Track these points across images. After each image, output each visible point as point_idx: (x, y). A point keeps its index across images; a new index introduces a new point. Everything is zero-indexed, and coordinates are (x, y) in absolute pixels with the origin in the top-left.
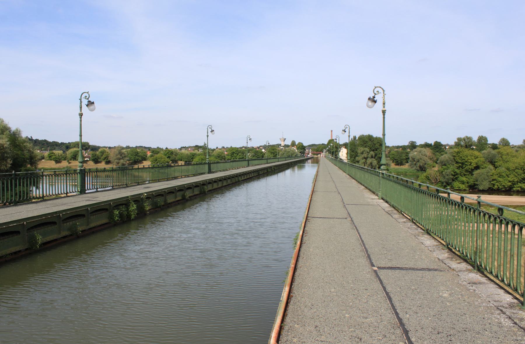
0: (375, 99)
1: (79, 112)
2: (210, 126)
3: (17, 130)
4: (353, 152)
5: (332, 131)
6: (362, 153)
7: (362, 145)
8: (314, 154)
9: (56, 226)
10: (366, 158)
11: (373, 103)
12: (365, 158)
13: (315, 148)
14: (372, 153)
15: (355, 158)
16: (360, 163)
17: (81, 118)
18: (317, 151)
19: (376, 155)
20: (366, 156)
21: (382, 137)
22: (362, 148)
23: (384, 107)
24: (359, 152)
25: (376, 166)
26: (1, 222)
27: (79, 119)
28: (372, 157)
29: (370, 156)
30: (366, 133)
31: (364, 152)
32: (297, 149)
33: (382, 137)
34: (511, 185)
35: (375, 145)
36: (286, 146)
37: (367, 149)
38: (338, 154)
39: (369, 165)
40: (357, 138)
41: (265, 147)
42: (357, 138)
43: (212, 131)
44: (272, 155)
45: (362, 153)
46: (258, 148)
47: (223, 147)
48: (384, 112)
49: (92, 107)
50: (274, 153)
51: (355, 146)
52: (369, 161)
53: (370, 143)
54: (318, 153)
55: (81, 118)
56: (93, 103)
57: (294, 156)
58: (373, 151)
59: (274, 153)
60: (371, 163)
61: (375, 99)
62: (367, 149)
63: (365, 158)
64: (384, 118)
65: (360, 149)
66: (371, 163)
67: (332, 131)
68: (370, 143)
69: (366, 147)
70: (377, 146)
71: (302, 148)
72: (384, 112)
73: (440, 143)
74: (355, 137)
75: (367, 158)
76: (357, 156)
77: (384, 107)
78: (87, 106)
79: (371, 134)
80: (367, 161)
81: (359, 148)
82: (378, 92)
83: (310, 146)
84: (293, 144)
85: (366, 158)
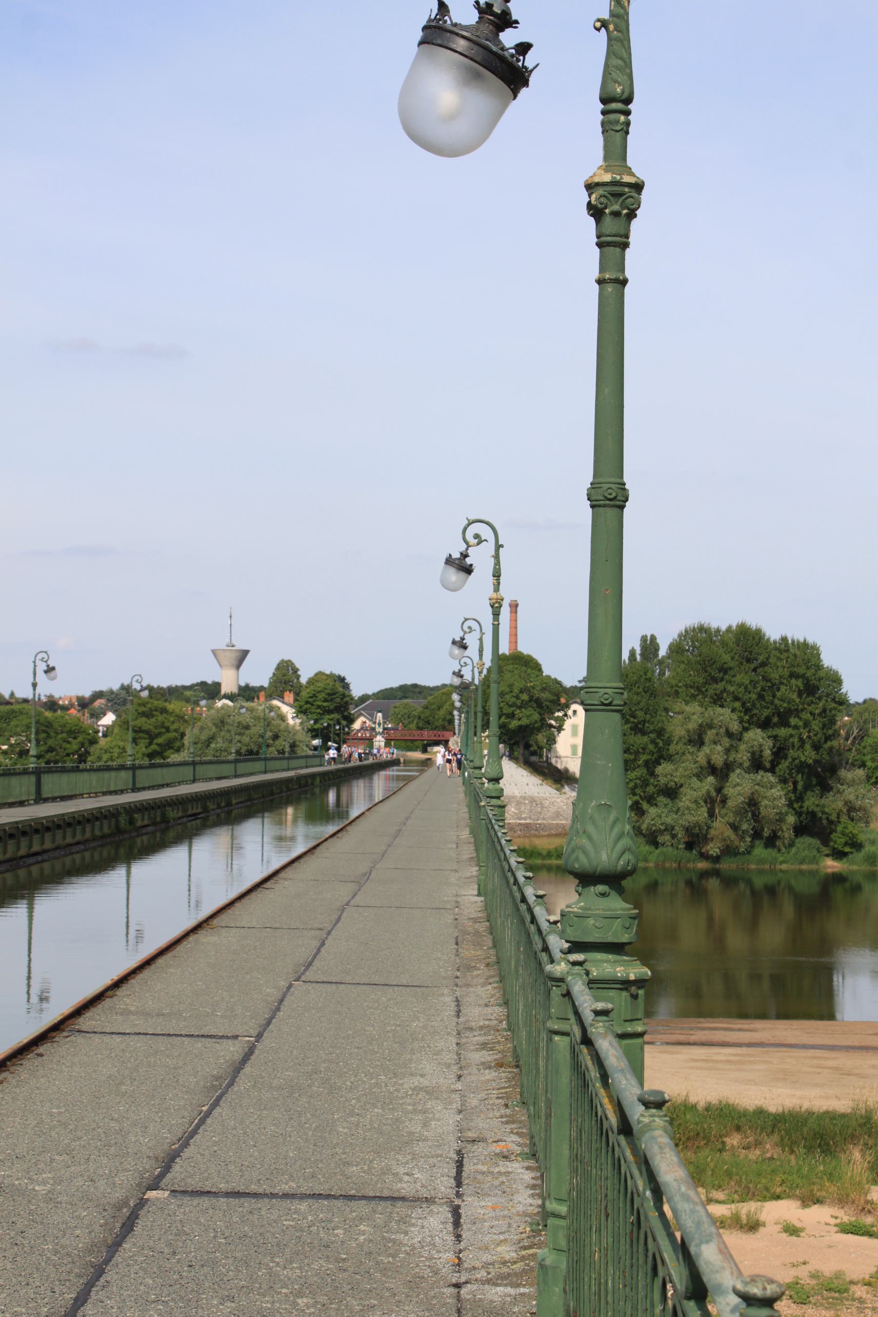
0: (468, 561)
1: (31, 680)
4: (638, 729)
5: (537, 65)
6: (697, 740)
7: (696, 692)
8: (409, 744)
10: (721, 772)
11: (462, 575)
12: (712, 769)
13: (416, 705)
14: (756, 736)
15: (650, 766)
16: (686, 800)
17: (613, 245)
18: (426, 723)
19: (779, 753)
20: (718, 760)
22: (694, 708)
23: (497, 588)
24: (677, 728)
25: (781, 820)
27: (589, 259)
28: (757, 764)
29: (743, 756)
30: (722, 617)
31: (710, 734)
32: (301, 711)
34: (803, 802)
35: (774, 687)
36: (247, 693)
37: (727, 716)
38: (552, 741)
39: (740, 812)
40: (663, 652)
41: (120, 699)
42: (663, 652)
43: (50, 670)
44: (142, 748)
45: (697, 740)
46: (84, 704)
48: (614, 205)
49: (52, 674)
50: (152, 737)
51: (651, 693)
52: (740, 786)
53: (743, 678)
54: (427, 735)
55: (613, 245)
56: (53, 669)
57: (272, 752)
58: (765, 725)
59: (152, 737)
60: (752, 803)
61: (468, 561)
62: (727, 716)
63: (712, 769)
64: (613, 283)
65: (684, 716)
66: (752, 803)
67: (537, 65)
68: (743, 678)
69: (718, 700)
70: (789, 693)
71: (331, 704)
72: (614, 205)
74: (649, 645)
75: (728, 767)
76: (662, 756)
78: (46, 672)
79: (753, 622)
80: (729, 791)
81: (679, 705)
82: (470, 628)
83: (388, 695)
84: (285, 678)
85: (721, 772)
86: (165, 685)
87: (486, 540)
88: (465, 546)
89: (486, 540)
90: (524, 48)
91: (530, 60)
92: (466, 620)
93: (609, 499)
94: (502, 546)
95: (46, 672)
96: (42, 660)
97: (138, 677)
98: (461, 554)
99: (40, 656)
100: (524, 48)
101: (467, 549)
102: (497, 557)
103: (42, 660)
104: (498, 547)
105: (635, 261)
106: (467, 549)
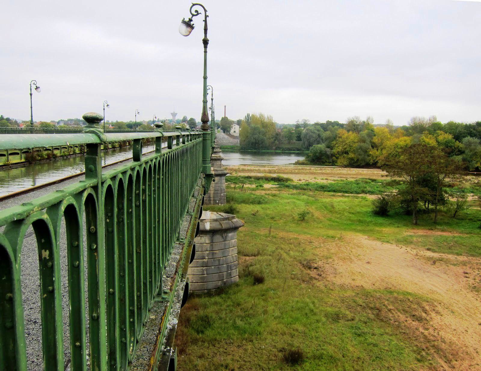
0: (192, 23)
2: (34, 82)
3: (369, 118)
5: (225, 107)
9: (19, 155)
11: (189, 29)
17: (206, 47)
21: (143, 153)
23: (212, 97)
26: (1, 149)
33: (143, 153)
43: (37, 88)
48: (206, 42)
55: (206, 47)
64: (205, 52)
67: (225, 107)
72: (206, 42)
73: (337, 122)
77: (212, 97)
78: (36, 89)
82: (196, 11)
86: (333, 121)
87: (200, 13)
88: (191, 16)
89: (200, 13)
90: (193, 24)
91: (194, 26)
92: (194, 5)
93: (31, 107)
94: (208, 16)
95: (36, 89)
97: (34, 82)
98: (189, 19)
99: (105, 102)
100: (193, 24)
101: (192, 18)
102: (205, 21)
104: (206, 16)
106: (192, 18)
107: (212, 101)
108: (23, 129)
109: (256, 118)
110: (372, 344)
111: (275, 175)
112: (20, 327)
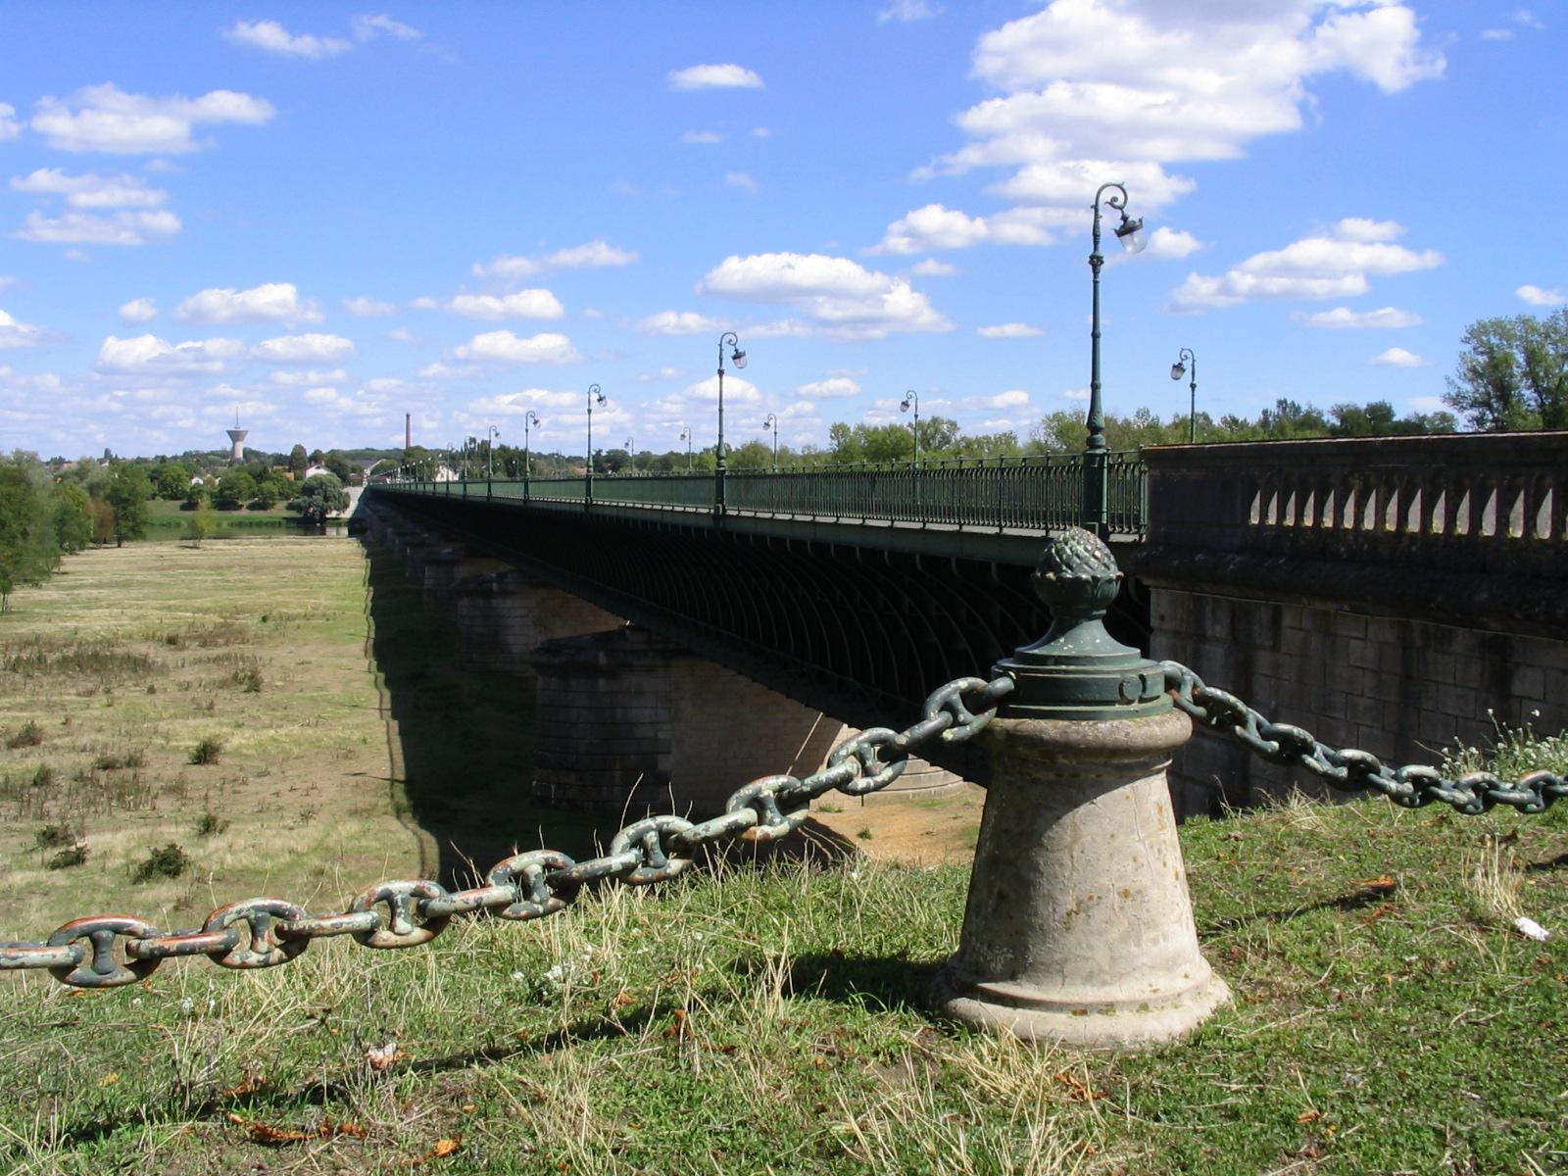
1: (1103, 268)
5: (408, 416)
17: (1193, 390)
23: (1096, 249)
43: (737, 356)
47: (299, 451)
48: (1193, 386)
55: (1096, 273)
67: (408, 416)
72: (1193, 386)
77: (1096, 249)
95: (735, 358)
96: (1112, 202)
99: (727, 338)
102: (1193, 366)
103: (595, 391)
105: (1100, 279)
107: (1096, 273)
108: (985, 464)
109: (1050, 809)
110: (1418, 951)
111: (287, 562)
112: (929, 403)
